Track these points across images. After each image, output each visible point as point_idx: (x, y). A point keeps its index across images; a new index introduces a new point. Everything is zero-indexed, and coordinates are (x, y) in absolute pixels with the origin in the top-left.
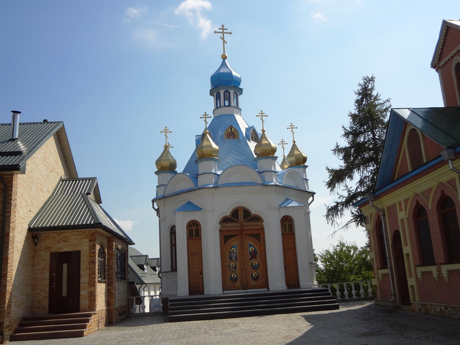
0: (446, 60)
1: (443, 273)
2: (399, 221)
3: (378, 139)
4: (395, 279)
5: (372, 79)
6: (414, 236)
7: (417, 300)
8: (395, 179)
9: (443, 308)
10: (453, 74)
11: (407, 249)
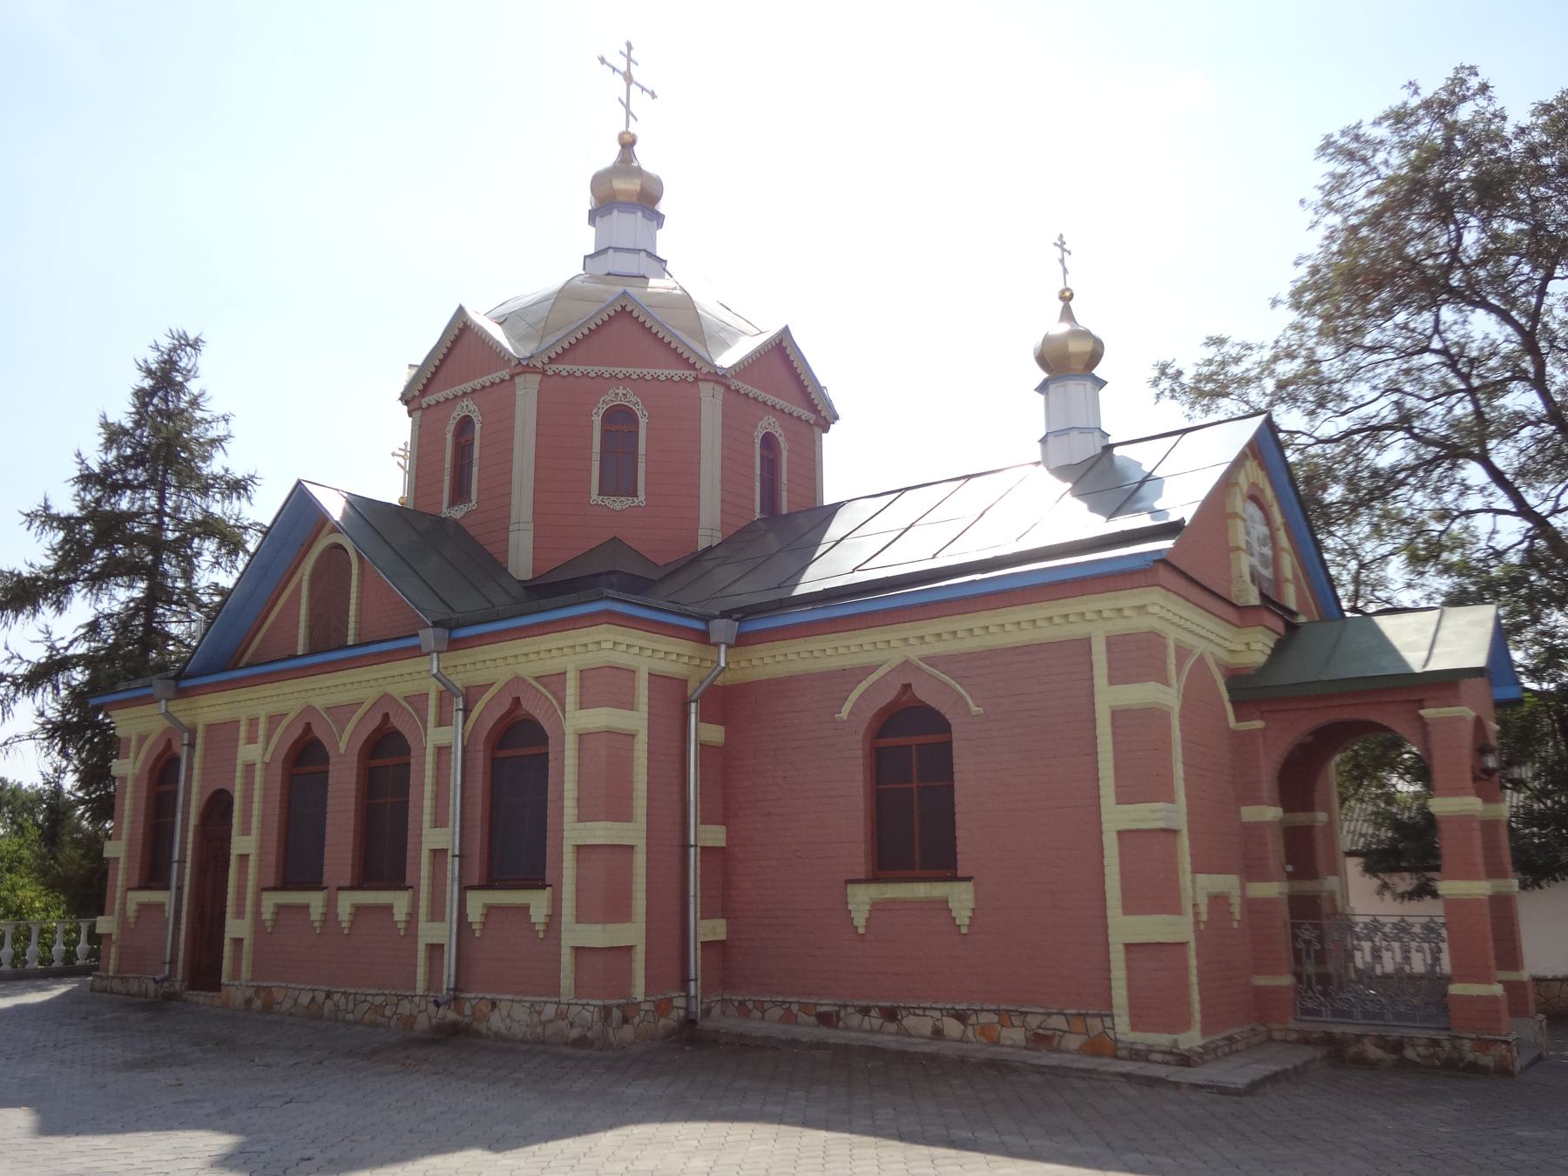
0: (441, 396)
1: (339, 910)
2: (239, 768)
3: (168, 515)
4: (184, 920)
5: (195, 345)
6: (277, 811)
7: (243, 975)
8: (245, 660)
9: (321, 996)
10: (449, 437)
11: (243, 843)
